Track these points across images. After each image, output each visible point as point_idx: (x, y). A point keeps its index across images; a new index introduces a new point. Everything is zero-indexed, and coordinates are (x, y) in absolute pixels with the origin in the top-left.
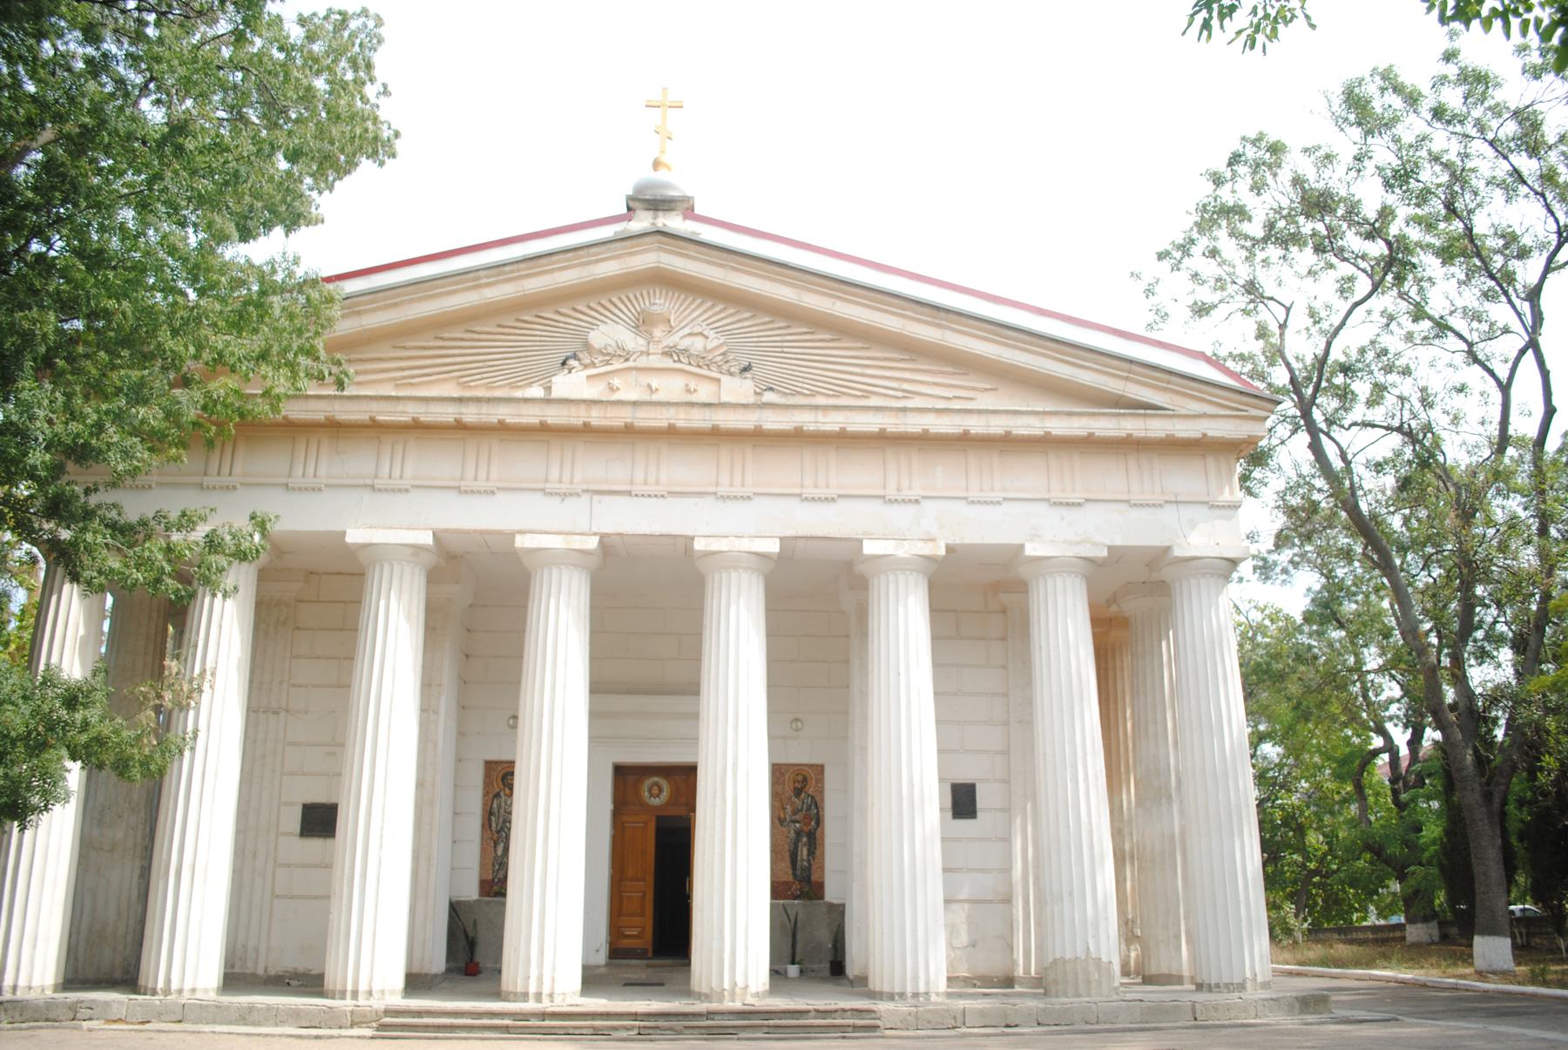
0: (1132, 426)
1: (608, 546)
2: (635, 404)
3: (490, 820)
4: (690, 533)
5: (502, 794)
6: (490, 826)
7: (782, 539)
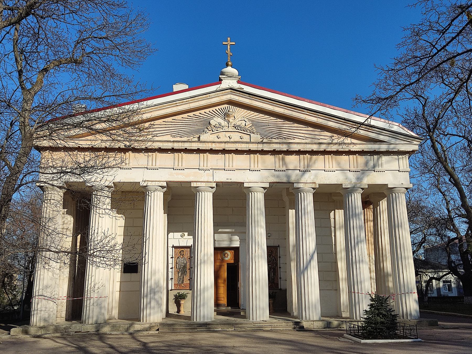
0: (375, 147)
1: (218, 184)
2: (225, 143)
3: (176, 265)
4: (242, 181)
5: (180, 257)
6: (177, 267)
7: (270, 183)
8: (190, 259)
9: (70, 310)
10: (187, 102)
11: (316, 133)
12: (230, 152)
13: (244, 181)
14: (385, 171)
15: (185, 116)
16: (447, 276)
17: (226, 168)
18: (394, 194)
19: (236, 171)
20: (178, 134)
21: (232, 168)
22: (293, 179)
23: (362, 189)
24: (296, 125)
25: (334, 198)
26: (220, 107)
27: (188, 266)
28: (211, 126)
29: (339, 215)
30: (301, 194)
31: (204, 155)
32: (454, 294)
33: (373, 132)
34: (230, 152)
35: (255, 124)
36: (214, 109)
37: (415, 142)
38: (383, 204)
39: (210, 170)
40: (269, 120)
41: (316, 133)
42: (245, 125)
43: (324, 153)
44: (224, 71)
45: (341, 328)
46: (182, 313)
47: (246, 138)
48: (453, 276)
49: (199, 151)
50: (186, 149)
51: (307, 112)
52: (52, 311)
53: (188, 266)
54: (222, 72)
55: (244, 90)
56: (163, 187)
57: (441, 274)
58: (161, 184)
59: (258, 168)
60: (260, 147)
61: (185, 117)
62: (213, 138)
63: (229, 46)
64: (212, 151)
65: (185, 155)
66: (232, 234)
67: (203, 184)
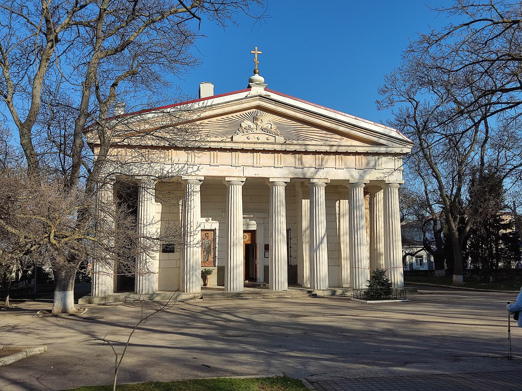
0: (376, 149)
1: (247, 178)
4: (268, 177)
7: (291, 178)
8: (214, 240)
9: (116, 284)
10: (222, 106)
11: (329, 136)
12: (258, 151)
13: (269, 177)
14: (384, 169)
15: (219, 118)
16: (421, 252)
17: (255, 165)
18: (390, 189)
19: (263, 168)
20: (213, 134)
21: (260, 165)
22: (308, 175)
23: (365, 184)
24: (313, 128)
25: (340, 190)
26: (249, 111)
27: (212, 247)
28: (242, 128)
29: (344, 205)
30: (315, 188)
31: (235, 154)
32: (425, 268)
33: (376, 137)
34: (258, 151)
35: (280, 127)
36: (244, 112)
37: (409, 146)
38: (380, 195)
39: (241, 166)
40: (291, 124)
41: (329, 136)
42: (271, 128)
43: (336, 153)
44: (253, 79)
45: (344, 295)
46: (208, 286)
47: (272, 139)
48: (425, 252)
49: (232, 150)
50: (221, 148)
51: (323, 118)
52: (110, 285)
53: (212, 247)
54: (251, 79)
55: (271, 97)
56: (200, 181)
57: (415, 250)
58: (199, 178)
59: (281, 166)
60: (284, 148)
61: (219, 119)
62: (243, 138)
63: (256, 55)
64: (243, 151)
65: (219, 153)
66: (251, 219)
67: (236, 179)
